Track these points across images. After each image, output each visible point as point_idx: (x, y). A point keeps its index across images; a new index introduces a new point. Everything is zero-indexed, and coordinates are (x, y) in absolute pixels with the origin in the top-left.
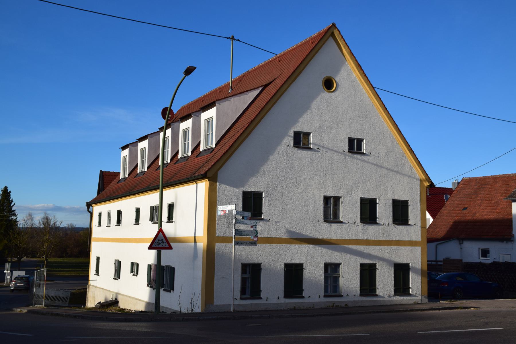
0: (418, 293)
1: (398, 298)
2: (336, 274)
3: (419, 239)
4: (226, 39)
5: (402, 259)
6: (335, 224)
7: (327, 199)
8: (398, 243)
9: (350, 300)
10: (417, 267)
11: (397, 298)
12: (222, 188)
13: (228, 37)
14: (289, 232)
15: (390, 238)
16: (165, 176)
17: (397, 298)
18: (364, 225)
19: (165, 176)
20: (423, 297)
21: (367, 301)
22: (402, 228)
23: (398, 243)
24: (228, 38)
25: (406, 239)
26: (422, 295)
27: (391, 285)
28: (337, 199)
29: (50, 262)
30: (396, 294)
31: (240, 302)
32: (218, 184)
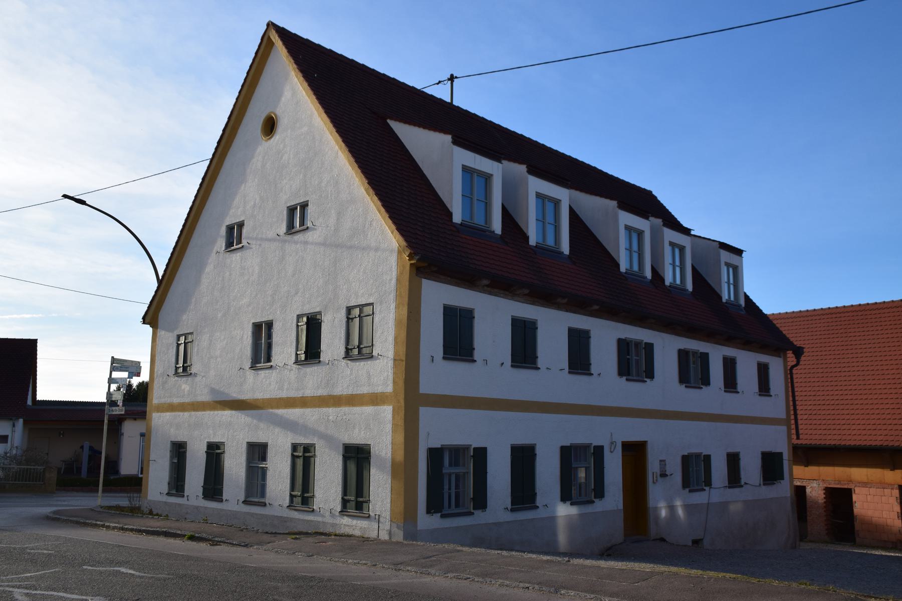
0: (383, 515)
1: (346, 520)
2: (264, 463)
3: (389, 389)
4: (436, 85)
5: (357, 437)
6: (262, 372)
7: (257, 327)
8: (352, 400)
9: (276, 515)
10: (383, 454)
11: (345, 520)
12: (161, 333)
13: (437, 82)
14: (213, 391)
15: (339, 391)
16: (805, 362)
17: (345, 520)
18: (300, 368)
19: (805, 362)
20: (394, 525)
21: (299, 520)
22: (524, 374)
23: (352, 400)
24: (438, 84)
25: (365, 390)
26: (391, 521)
27: (336, 491)
28: (270, 325)
29: (452, 475)
30: (344, 511)
31: (165, 499)
32: (159, 330)
